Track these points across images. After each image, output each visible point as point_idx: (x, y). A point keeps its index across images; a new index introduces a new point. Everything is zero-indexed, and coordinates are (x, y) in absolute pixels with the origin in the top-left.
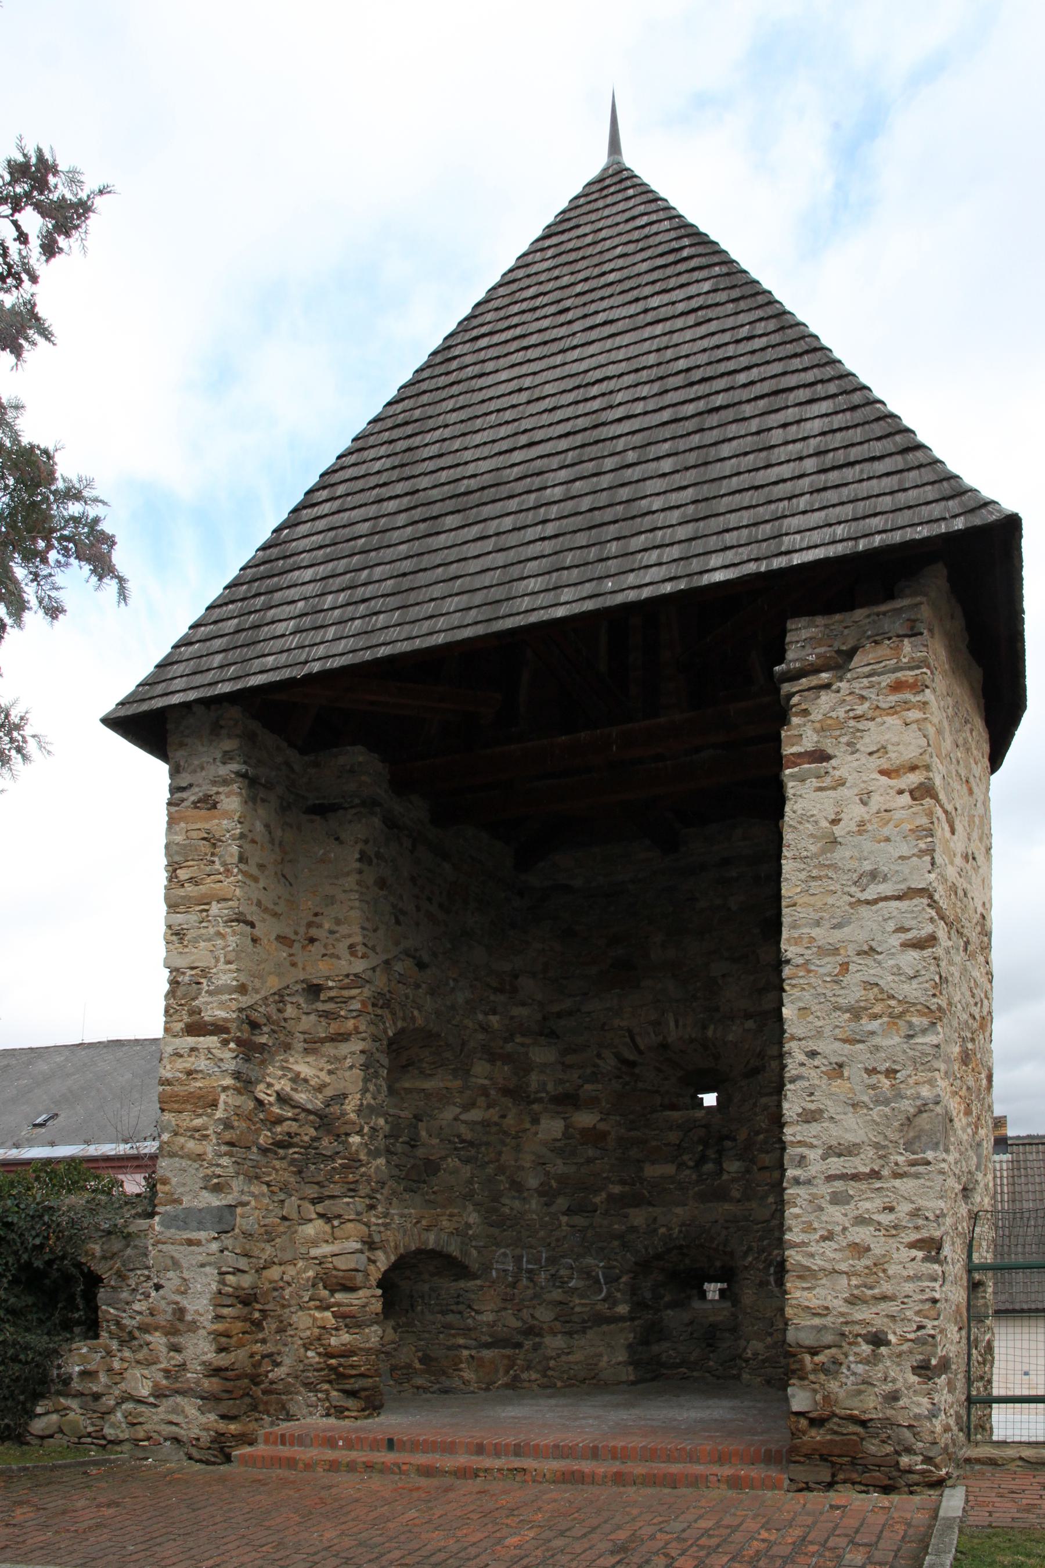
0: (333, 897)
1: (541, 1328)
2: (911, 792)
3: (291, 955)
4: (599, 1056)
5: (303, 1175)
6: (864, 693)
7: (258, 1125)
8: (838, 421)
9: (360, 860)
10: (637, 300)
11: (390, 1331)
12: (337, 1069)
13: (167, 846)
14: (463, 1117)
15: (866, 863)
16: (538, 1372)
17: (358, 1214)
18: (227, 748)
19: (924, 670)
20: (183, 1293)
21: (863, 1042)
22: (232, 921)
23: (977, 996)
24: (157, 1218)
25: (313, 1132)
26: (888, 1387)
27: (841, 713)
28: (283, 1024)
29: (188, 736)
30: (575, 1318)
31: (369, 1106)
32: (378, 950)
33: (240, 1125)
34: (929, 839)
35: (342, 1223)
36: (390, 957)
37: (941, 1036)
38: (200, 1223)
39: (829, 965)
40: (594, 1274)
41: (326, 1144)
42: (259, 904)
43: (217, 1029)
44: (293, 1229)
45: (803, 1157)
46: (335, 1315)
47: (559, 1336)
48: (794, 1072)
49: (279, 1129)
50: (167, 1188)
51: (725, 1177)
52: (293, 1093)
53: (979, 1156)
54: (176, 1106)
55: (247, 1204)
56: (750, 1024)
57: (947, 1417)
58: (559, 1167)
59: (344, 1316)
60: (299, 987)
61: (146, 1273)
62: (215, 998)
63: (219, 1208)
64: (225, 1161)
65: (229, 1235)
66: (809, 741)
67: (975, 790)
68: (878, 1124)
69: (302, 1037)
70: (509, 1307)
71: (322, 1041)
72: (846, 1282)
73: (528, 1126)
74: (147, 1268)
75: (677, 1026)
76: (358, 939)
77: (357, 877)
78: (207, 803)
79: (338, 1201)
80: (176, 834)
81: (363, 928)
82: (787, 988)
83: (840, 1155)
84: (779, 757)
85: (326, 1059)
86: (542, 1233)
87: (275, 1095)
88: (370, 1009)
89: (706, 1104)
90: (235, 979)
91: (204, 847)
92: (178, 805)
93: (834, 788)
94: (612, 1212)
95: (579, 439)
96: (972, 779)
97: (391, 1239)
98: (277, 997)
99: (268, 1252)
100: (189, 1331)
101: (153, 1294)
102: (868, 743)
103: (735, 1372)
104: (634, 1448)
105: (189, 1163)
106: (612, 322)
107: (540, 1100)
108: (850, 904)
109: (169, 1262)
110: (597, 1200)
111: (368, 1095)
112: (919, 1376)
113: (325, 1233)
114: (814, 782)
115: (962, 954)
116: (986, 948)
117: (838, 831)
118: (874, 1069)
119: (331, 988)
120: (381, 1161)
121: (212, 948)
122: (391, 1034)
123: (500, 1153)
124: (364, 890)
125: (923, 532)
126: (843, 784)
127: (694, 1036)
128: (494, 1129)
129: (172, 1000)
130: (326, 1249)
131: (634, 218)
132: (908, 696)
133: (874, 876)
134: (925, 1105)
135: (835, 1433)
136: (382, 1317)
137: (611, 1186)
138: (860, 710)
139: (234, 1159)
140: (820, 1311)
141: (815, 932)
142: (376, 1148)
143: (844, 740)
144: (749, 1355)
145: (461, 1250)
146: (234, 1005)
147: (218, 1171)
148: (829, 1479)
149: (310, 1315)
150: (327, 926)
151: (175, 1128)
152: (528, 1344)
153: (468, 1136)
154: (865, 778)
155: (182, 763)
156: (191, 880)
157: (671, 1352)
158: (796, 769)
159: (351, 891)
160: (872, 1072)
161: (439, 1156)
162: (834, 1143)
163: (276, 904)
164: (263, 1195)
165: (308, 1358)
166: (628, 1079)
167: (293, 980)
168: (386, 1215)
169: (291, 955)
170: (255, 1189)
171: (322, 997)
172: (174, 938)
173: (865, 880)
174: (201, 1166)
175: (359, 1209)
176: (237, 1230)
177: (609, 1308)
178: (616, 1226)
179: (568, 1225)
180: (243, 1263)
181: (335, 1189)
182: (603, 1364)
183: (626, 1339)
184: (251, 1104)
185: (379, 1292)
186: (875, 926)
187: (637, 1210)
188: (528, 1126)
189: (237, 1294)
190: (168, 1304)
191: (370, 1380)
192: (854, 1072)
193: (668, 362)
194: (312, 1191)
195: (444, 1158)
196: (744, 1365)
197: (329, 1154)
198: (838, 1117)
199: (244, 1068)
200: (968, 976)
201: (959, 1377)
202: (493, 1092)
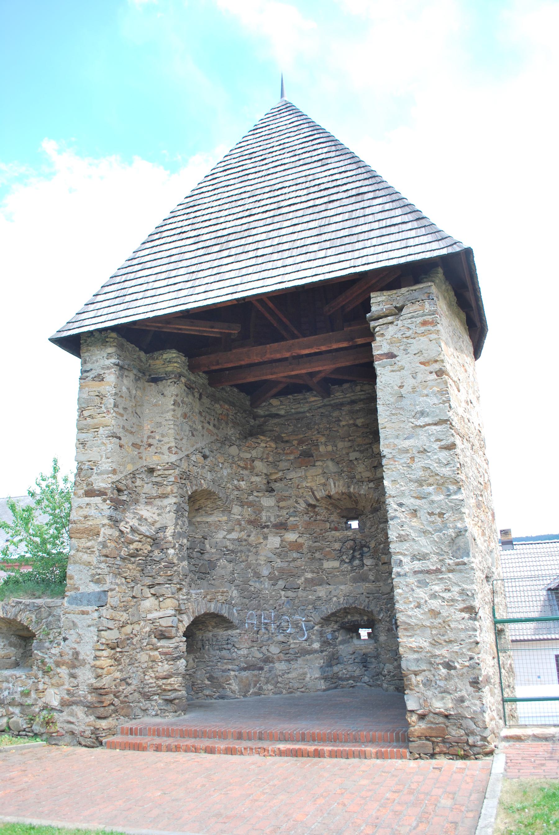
0: (161, 423)
1: (273, 658)
2: (436, 373)
3: (139, 453)
4: (296, 502)
5: (144, 572)
6: (409, 326)
7: (121, 545)
8: (387, 207)
9: (174, 404)
10: (295, 155)
11: (191, 661)
12: (162, 513)
13: (78, 400)
14: (228, 537)
15: (417, 407)
16: (272, 684)
17: (173, 594)
18: (110, 352)
19: (436, 316)
20: (78, 643)
21: (426, 498)
22: (110, 437)
23: (481, 472)
24: (66, 599)
25: (149, 548)
26: (458, 694)
27: (399, 335)
28: (135, 489)
29: (90, 346)
30: (291, 651)
31: (179, 532)
32: (183, 449)
33: (111, 545)
34: (447, 396)
35: (164, 599)
36: (189, 452)
37: (464, 495)
38: (89, 601)
39: (405, 458)
40: (300, 625)
41: (156, 554)
42: (123, 427)
43: (101, 493)
44: (138, 603)
45: (401, 561)
46: (161, 653)
47: (283, 662)
48: (393, 515)
49: (131, 547)
50: (71, 582)
51: (365, 568)
52: (139, 527)
53: (493, 558)
54: (78, 535)
55: (114, 589)
56: (371, 485)
57: (492, 711)
58: (279, 563)
59: (165, 654)
60: (143, 469)
61: (59, 630)
62: (100, 477)
63: (99, 593)
64: (103, 565)
65: (104, 608)
66: (385, 349)
67: (468, 370)
68: (437, 542)
69: (144, 496)
70: (255, 645)
71: (155, 498)
72: (430, 632)
73: (262, 541)
74: (60, 628)
75: (335, 486)
76: (173, 444)
77: (173, 413)
78: (100, 378)
79: (162, 586)
80: (83, 393)
81: (175, 439)
82: (385, 470)
83: (419, 560)
84: (372, 356)
85: (156, 508)
86: (271, 602)
87: (130, 528)
88: (179, 480)
89: (353, 527)
90: (110, 467)
91: (97, 400)
92: (85, 379)
93: (399, 371)
94: (308, 589)
95: (271, 214)
96: (465, 364)
97: (190, 607)
98: (132, 475)
99: (124, 617)
100: (81, 665)
101: (62, 643)
102: (413, 349)
103: (379, 683)
104: (324, 734)
105: (84, 567)
106: (285, 164)
107: (267, 527)
108: (412, 427)
109: (71, 624)
110: (299, 582)
111: (178, 527)
112: (474, 687)
113: (155, 605)
114: (389, 368)
115: (471, 451)
116: (482, 447)
117: (403, 391)
118: (432, 513)
119: (159, 470)
120: (185, 563)
121: (99, 451)
122: (190, 493)
123: (248, 556)
124: (176, 420)
125: (428, 255)
126: (403, 369)
127: (343, 491)
128: (244, 543)
129: (78, 478)
130: (155, 615)
131: (293, 122)
132: (430, 327)
133: (422, 413)
134: (460, 532)
135: (432, 723)
136: (186, 653)
137: (306, 574)
138: (408, 334)
139: (107, 565)
140: (418, 650)
141: (396, 441)
142: (183, 556)
143: (402, 348)
144: (386, 673)
145: (229, 613)
146: (110, 480)
147: (99, 571)
148: (431, 752)
149: (147, 654)
150: (157, 438)
151: (77, 547)
152: (266, 668)
153: (231, 547)
154: (414, 366)
155: (87, 359)
156: (90, 416)
157: (344, 671)
158: (380, 362)
159: (170, 420)
160: (431, 514)
161: (216, 558)
162: (416, 553)
163: (132, 427)
164: (122, 584)
165: (146, 680)
166: (312, 514)
167: (140, 466)
168: (188, 594)
169: (139, 453)
170: (118, 581)
171: (155, 474)
172: (81, 446)
173: (418, 415)
174: (90, 568)
175: (173, 591)
176: (108, 605)
177: (309, 645)
178: (310, 597)
179: (285, 596)
180: (111, 624)
181: (160, 580)
182: (307, 679)
183: (319, 664)
184: (117, 533)
185: (185, 639)
186: (425, 438)
187: (321, 587)
188: (262, 541)
189: (107, 643)
190: (70, 649)
191: (180, 693)
192: (422, 514)
193: (310, 181)
194: (148, 581)
195: (218, 560)
196: (383, 678)
197: (158, 560)
198: (417, 539)
199: (114, 514)
200: (475, 462)
201: (496, 686)
202: (243, 523)
